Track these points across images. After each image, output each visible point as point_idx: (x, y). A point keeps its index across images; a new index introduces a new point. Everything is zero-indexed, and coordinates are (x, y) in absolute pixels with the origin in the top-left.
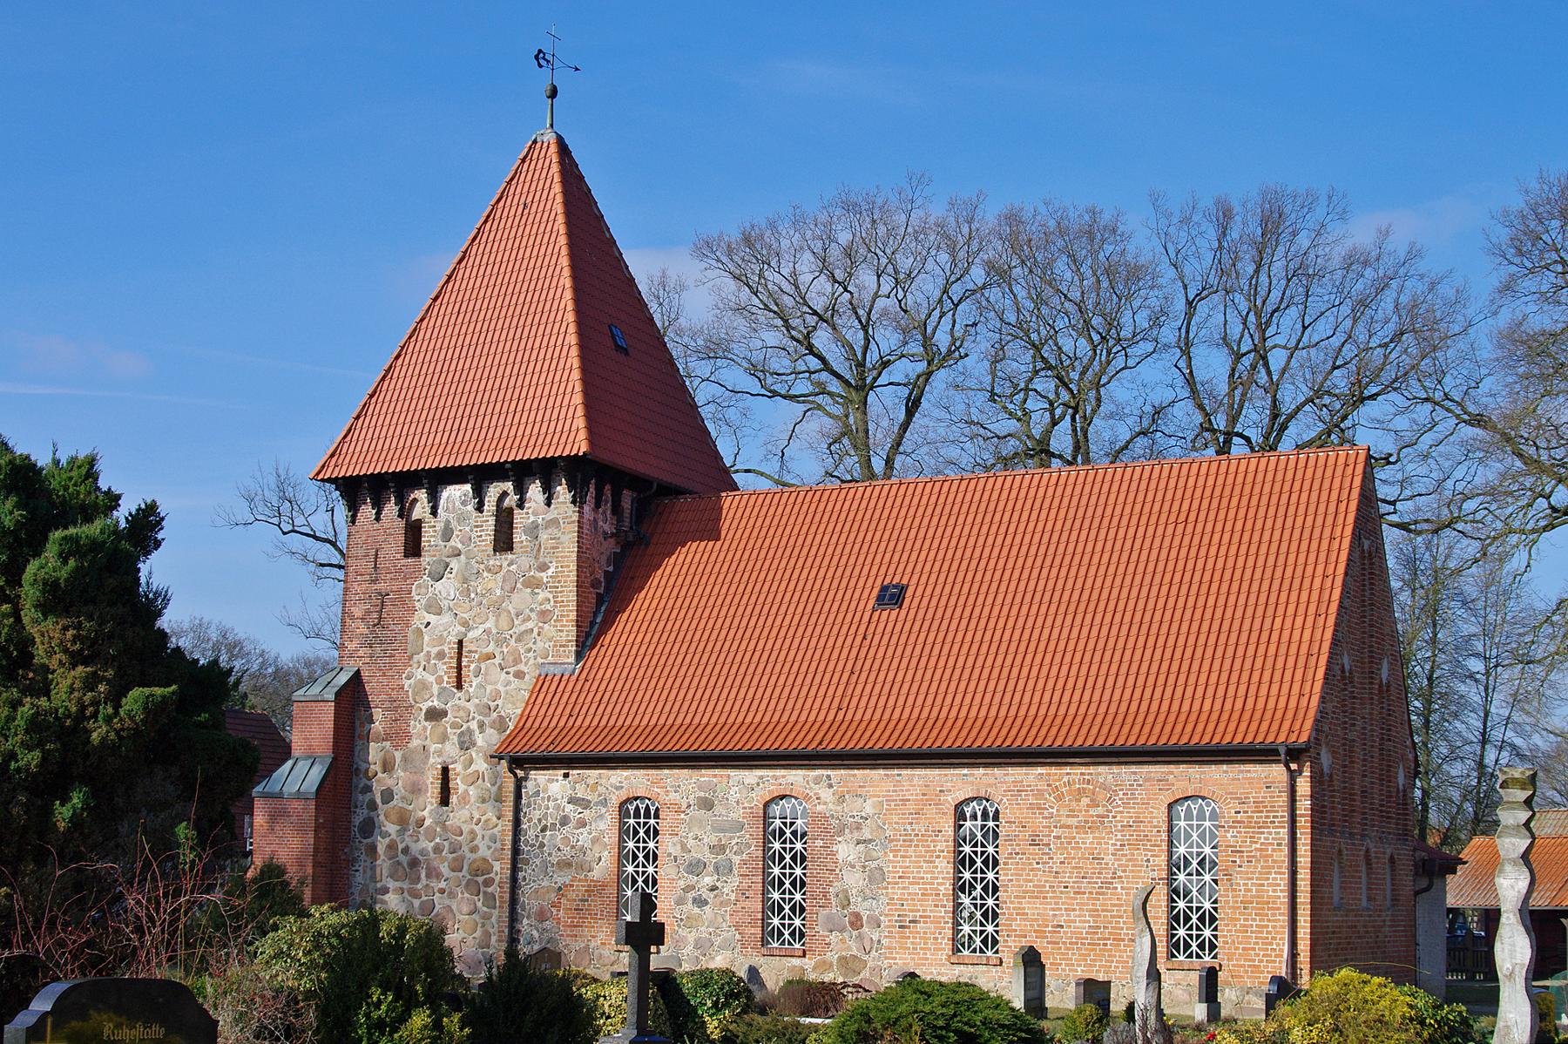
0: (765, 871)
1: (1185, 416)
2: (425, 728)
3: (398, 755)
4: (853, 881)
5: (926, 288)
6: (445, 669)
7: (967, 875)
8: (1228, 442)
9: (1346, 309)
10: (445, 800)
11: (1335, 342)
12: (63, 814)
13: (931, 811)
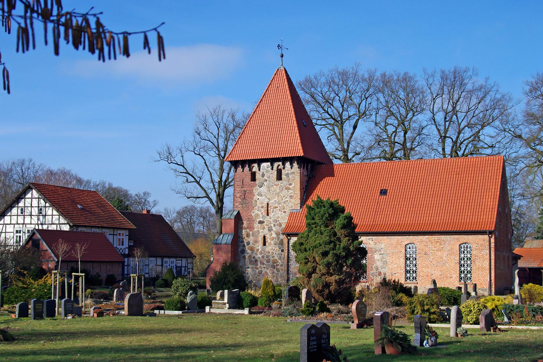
4: (379, 264)
6: (264, 211)
10: (264, 244)
13: (399, 247)
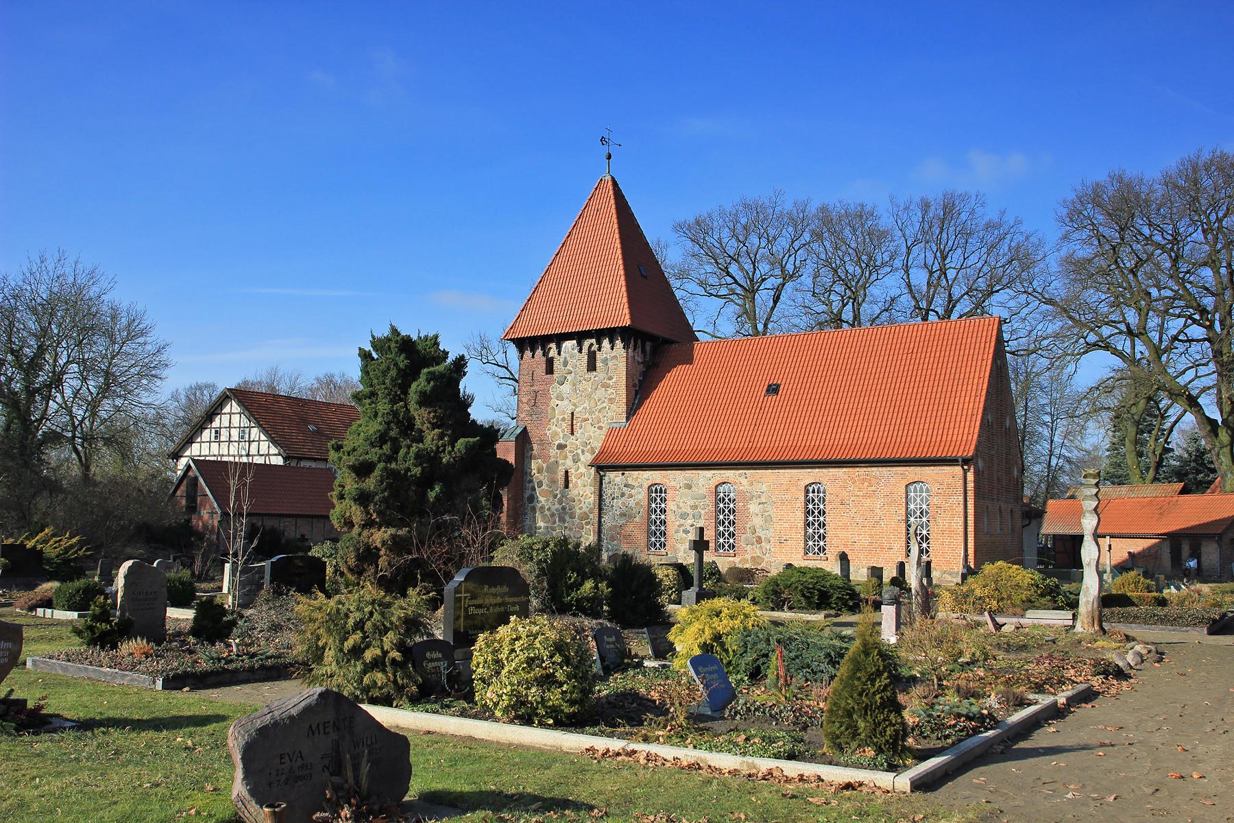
0: (716, 518)
1: (906, 301)
4: (757, 521)
5: (783, 243)
6: (565, 426)
7: (811, 519)
8: (927, 314)
9: (984, 250)
10: (567, 486)
11: (979, 265)
12: (432, 495)
13: (793, 489)
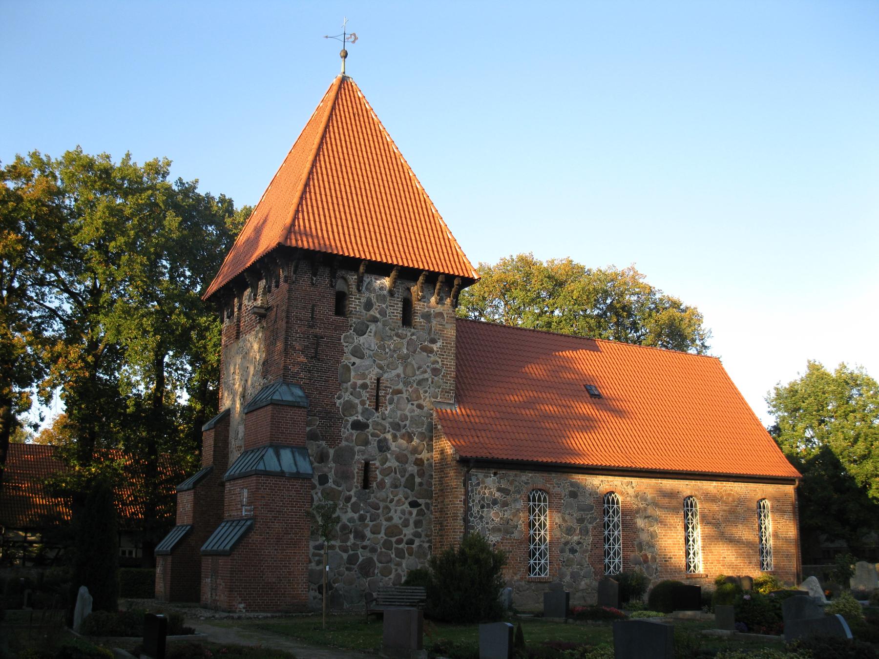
2: (352, 434)
3: (331, 452)
